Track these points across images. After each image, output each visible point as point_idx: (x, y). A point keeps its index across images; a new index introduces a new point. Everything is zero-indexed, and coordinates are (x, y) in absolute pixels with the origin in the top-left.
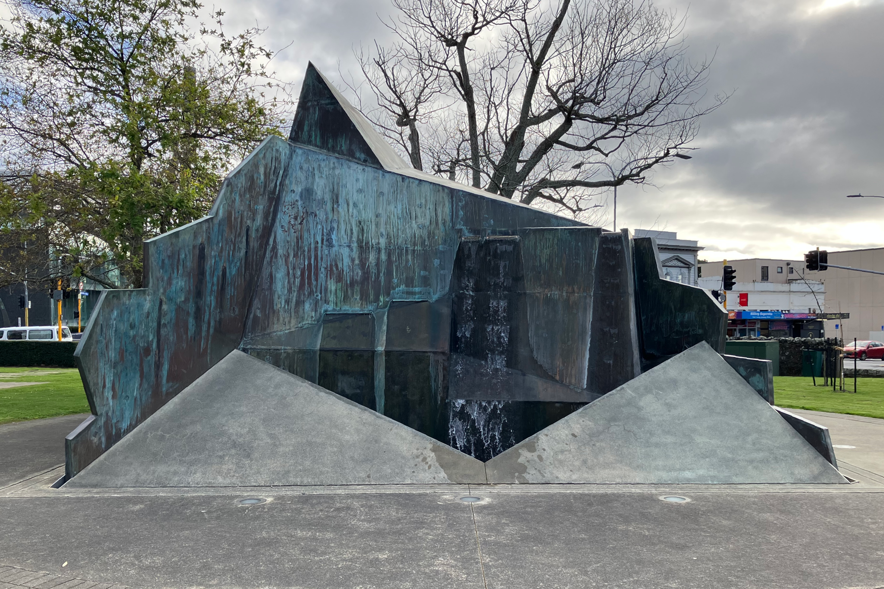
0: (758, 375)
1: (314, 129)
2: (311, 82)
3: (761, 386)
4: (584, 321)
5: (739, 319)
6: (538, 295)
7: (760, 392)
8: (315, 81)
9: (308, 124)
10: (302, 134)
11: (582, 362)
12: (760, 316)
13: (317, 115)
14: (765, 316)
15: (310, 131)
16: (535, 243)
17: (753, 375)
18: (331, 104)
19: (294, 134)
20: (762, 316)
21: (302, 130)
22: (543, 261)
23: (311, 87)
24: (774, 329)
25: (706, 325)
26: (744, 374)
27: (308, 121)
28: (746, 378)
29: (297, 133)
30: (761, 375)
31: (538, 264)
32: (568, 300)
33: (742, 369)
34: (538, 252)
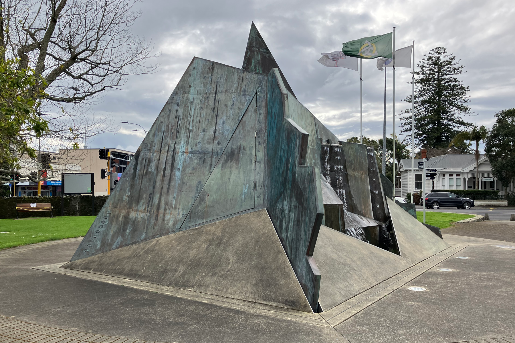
0: (412, 209)
1: (258, 66)
2: (254, 35)
3: (413, 214)
4: (368, 188)
5: (45, 185)
6: (352, 175)
7: (413, 216)
8: (256, 35)
9: (255, 62)
10: (250, 67)
11: (370, 207)
12: (55, 183)
13: (259, 57)
14: (58, 183)
15: (255, 66)
16: (348, 149)
17: (410, 209)
18: (267, 53)
19: (245, 65)
20: (57, 183)
21: (251, 65)
22: (352, 158)
23: (254, 38)
24: (59, 191)
25: (386, 189)
26: (406, 209)
27: (254, 60)
28: (407, 211)
29: (247, 65)
30: (413, 209)
31: (350, 160)
32: (361, 178)
33: (404, 207)
34: (350, 154)
